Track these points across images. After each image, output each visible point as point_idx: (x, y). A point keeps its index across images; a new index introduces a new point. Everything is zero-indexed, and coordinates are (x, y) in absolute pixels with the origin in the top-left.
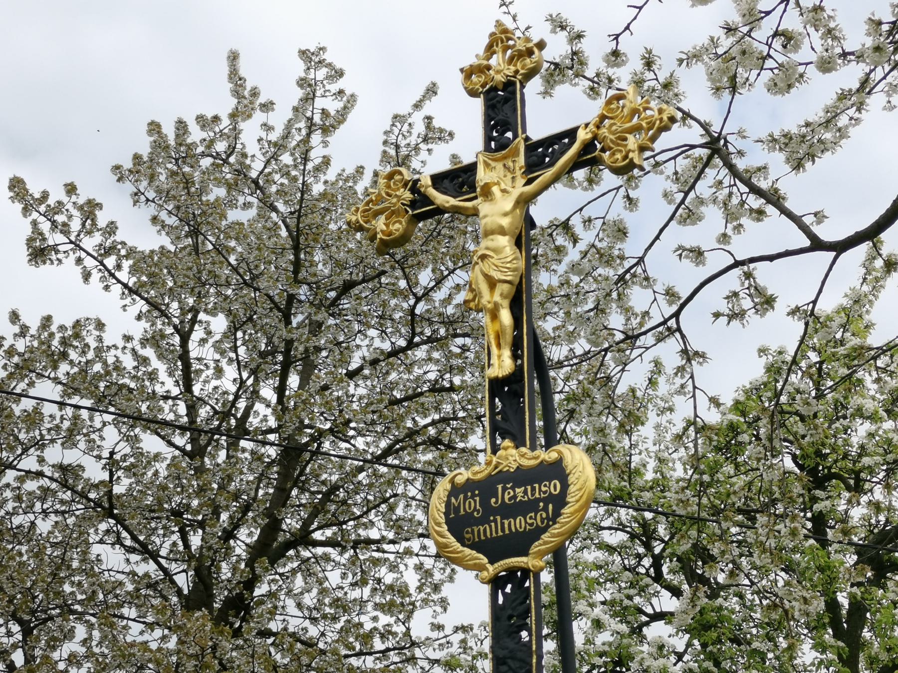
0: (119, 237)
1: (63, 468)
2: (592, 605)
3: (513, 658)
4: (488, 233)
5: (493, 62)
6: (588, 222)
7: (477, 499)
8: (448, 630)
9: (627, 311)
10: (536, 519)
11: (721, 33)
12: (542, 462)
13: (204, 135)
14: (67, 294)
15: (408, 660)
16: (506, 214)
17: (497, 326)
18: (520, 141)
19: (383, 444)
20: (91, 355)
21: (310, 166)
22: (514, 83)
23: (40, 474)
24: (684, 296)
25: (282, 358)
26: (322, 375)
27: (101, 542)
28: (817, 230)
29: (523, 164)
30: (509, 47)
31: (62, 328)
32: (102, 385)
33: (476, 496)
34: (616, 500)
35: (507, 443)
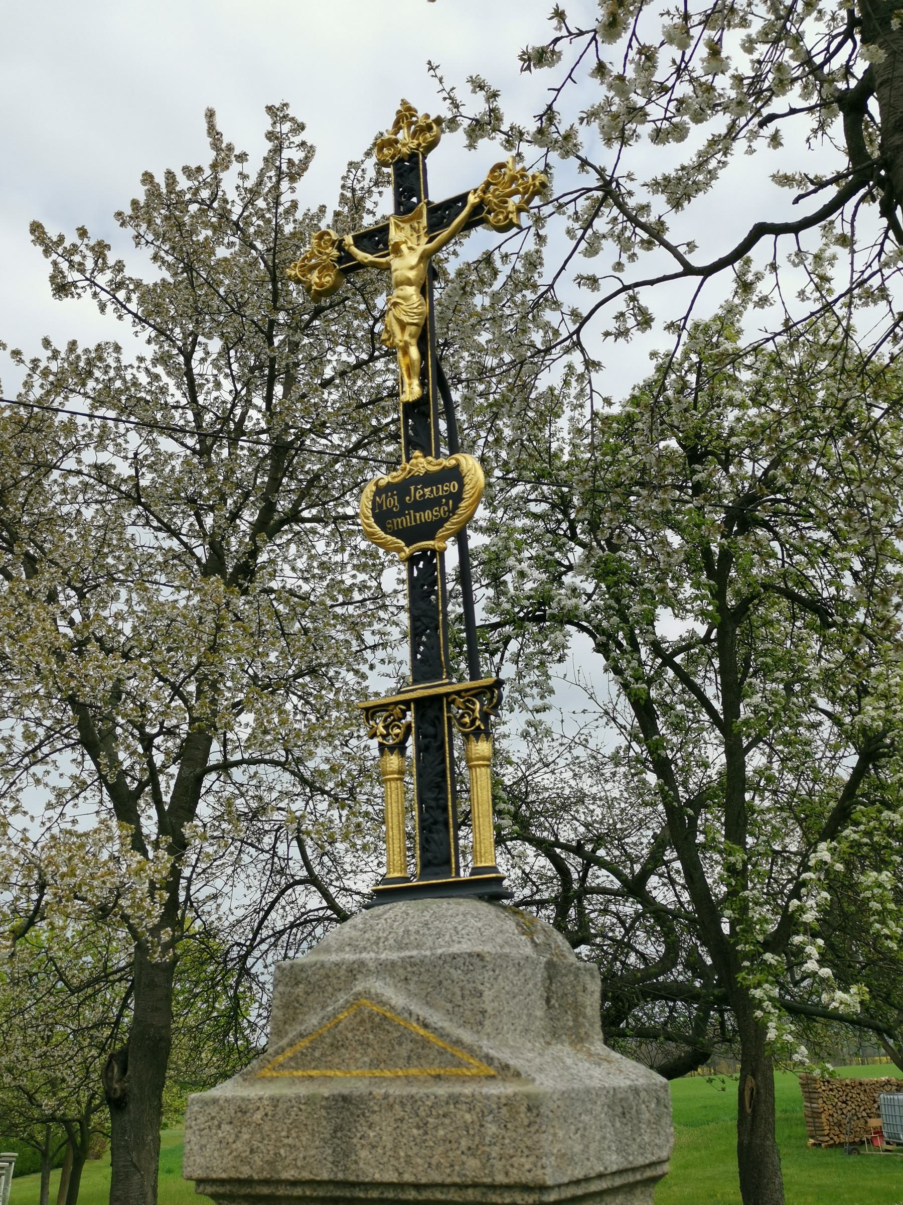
0: (128, 273)
1: (96, 466)
2: (520, 561)
4: (399, 284)
6: (505, 257)
10: (441, 511)
13: (190, 184)
14: (87, 322)
15: (380, 608)
16: (412, 268)
19: (354, 438)
20: (112, 373)
21: (281, 209)
22: (416, 155)
23: (79, 473)
24: (585, 315)
27: (134, 524)
28: (688, 257)
30: (413, 123)
31: (87, 351)
32: (123, 398)
35: (417, 453)
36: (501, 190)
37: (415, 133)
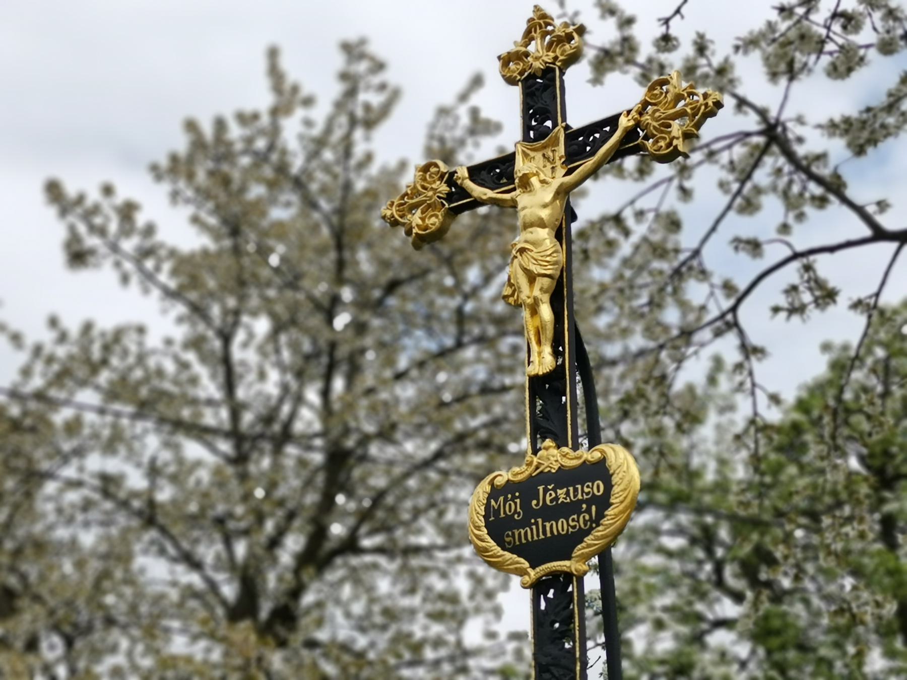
3: (557, 665)
4: (526, 226)
5: (532, 48)
7: (518, 501)
8: (503, 636)
9: (684, 305)
10: (580, 521)
11: (774, 16)
12: (584, 462)
14: (108, 300)
16: (545, 206)
17: (537, 322)
18: (560, 129)
19: (433, 446)
22: (553, 70)
24: (742, 286)
25: (327, 360)
26: (368, 379)
29: (563, 153)
30: (548, 33)
33: (517, 498)
34: (674, 503)
36: (662, 111)
37: (550, 44)
